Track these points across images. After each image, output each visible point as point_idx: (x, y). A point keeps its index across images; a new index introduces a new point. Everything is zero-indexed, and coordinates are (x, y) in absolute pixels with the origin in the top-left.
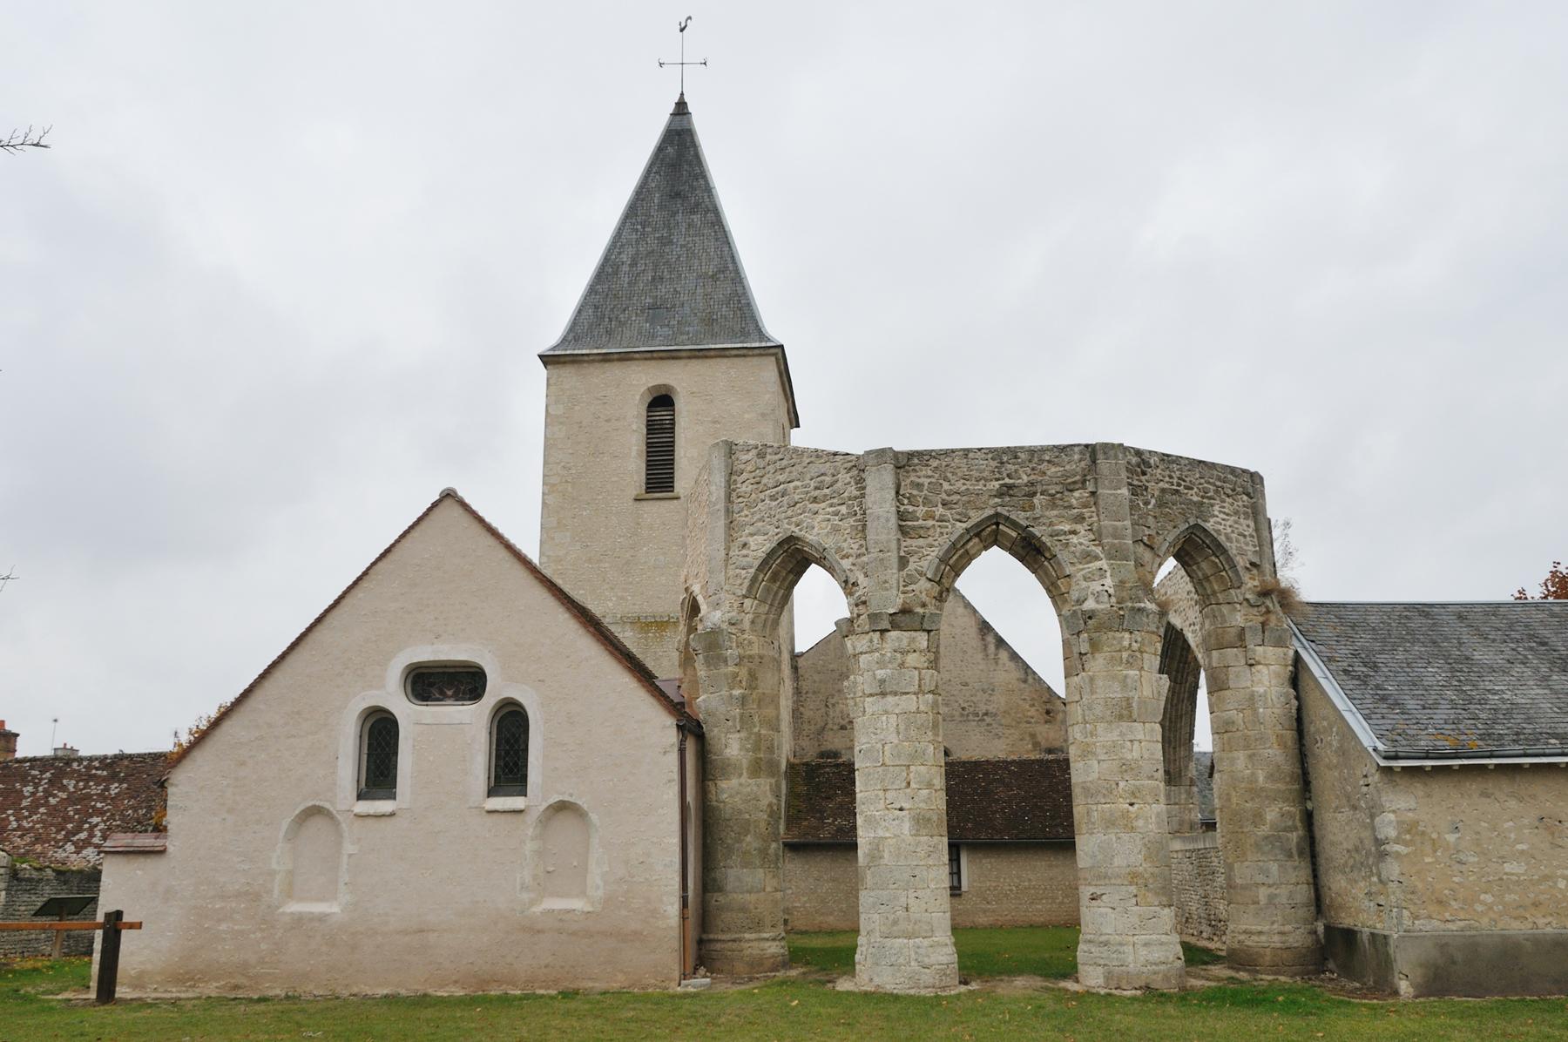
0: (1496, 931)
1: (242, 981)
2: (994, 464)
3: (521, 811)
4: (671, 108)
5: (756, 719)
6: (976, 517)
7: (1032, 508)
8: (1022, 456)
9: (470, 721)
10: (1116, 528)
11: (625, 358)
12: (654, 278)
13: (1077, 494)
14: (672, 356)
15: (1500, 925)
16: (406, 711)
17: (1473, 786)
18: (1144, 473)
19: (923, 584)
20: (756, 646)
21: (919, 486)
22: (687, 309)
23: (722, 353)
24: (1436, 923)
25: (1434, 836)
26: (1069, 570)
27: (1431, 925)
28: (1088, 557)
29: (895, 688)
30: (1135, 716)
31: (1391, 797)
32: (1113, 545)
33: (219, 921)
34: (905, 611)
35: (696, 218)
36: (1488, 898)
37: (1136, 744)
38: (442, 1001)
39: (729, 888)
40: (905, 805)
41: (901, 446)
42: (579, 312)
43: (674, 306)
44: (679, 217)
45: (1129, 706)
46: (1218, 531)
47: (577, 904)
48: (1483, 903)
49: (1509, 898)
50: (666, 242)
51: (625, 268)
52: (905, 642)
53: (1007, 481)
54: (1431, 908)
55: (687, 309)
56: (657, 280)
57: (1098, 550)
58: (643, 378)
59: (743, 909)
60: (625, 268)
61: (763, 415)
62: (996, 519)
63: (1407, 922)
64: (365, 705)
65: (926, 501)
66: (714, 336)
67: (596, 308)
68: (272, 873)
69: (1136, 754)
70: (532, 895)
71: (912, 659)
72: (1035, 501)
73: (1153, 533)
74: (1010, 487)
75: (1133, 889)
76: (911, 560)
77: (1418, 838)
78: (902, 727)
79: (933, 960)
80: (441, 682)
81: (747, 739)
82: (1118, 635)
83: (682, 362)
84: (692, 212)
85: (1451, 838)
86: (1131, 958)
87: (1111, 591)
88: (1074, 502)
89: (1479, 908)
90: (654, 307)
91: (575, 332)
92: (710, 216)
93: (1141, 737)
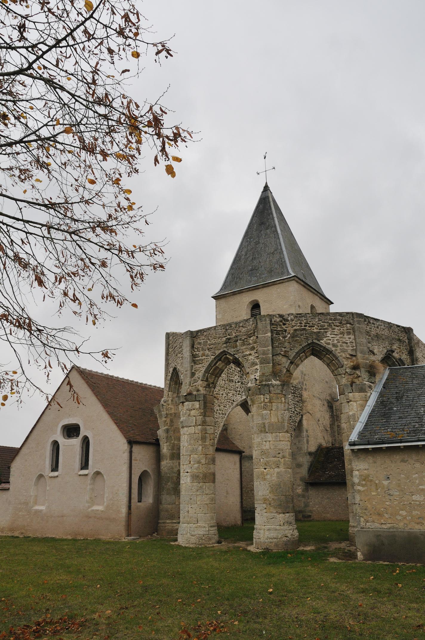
0: (407, 529)
1: (23, 531)
2: (224, 330)
3: (87, 475)
4: (262, 189)
5: (173, 438)
6: (218, 352)
7: (236, 346)
8: (233, 326)
9: (76, 442)
10: (264, 351)
11: (240, 292)
12: (252, 259)
13: (252, 338)
14: (256, 288)
15: (409, 527)
16: (62, 441)
17: (397, 457)
18: (284, 324)
19: (200, 382)
20: (173, 410)
21: (200, 343)
22: (263, 268)
23: (274, 283)
24: (377, 525)
25: (377, 482)
26: (248, 370)
27: (374, 525)
28: (254, 364)
29: (187, 424)
30: (267, 430)
31: (357, 463)
32: (263, 358)
33: (20, 511)
34: (190, 394)
35: (268, 231)
36: (404, 513)
37: (268, 442)
38: (66, 540)
39: (163, 502)
40: (189, 471)
41: (194, 329)
42: (227, 277)
43: (258, 268)
44: (262, 232)
45: (264, 427)
46: (329, 344)
47: (100, 508)
48: (400, 515)
49: (414, 513)
50: (257, 243)
51: (243, 257)
52: (190, 406)
53: (228, 337)
54: (374, 517)
55: (263, 268)
56: (254, 259)
57: (257, 361)
58: (247, 299)
59: (167, 511)
60: (243, 257)
61: (291, 305)
62: (224, 353)
63: (362, 524)
64: (52, 440)
65: (203, 349)
66: (272, 277)
67: (233, 274)
68: (31, 496)
69: (267, 447)
70: (89, 504)
71: (193, 413)
72: (238, 343)
73: (288, 350)
74: (229, 339)
75: (265, 505)
76: (197, 373)
77: (368, 483)
78: (188, 440)
79: (196, 533)
80: (71, 431)
81: (170, 445)
82: (259, 396)
83: (260, 290)
84: (267, 229)
85: (386, 483)
86: (262, 536)
87: (258, 378)
88: (251, 342)
89: (399, 518)
90: (252, 270)
91: (225, 286)
92: (273, 229)
93: (270, 439)
